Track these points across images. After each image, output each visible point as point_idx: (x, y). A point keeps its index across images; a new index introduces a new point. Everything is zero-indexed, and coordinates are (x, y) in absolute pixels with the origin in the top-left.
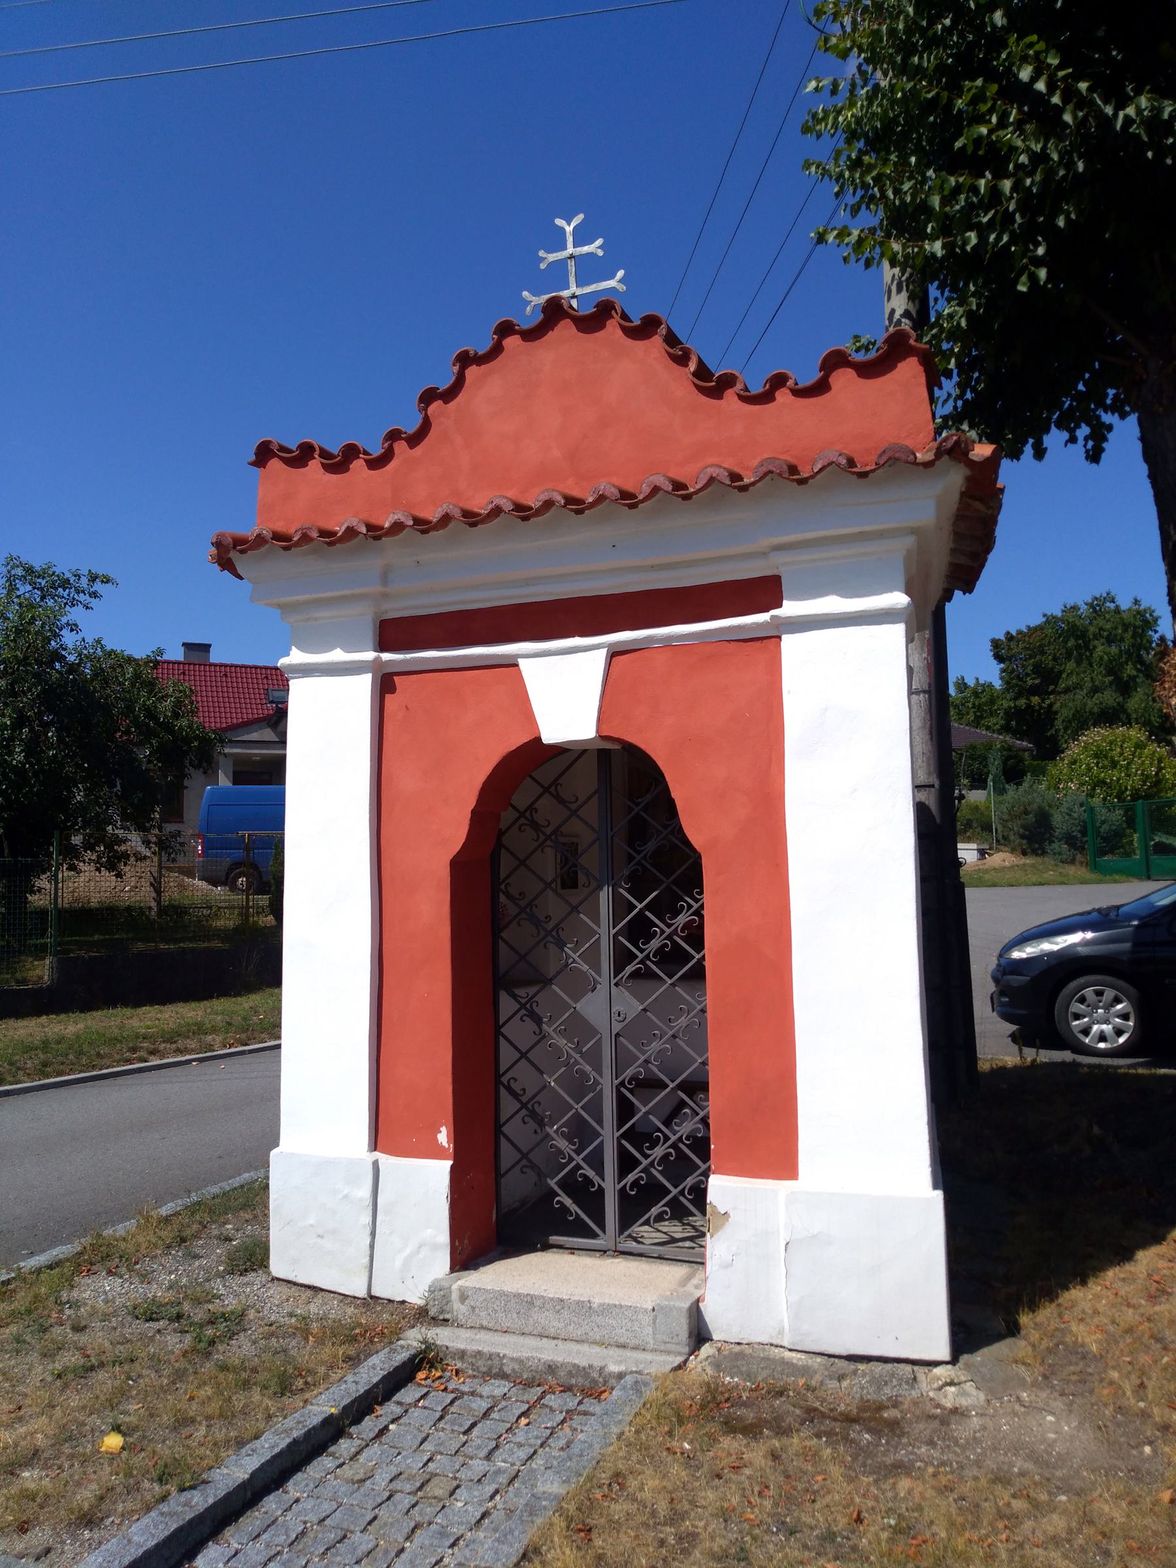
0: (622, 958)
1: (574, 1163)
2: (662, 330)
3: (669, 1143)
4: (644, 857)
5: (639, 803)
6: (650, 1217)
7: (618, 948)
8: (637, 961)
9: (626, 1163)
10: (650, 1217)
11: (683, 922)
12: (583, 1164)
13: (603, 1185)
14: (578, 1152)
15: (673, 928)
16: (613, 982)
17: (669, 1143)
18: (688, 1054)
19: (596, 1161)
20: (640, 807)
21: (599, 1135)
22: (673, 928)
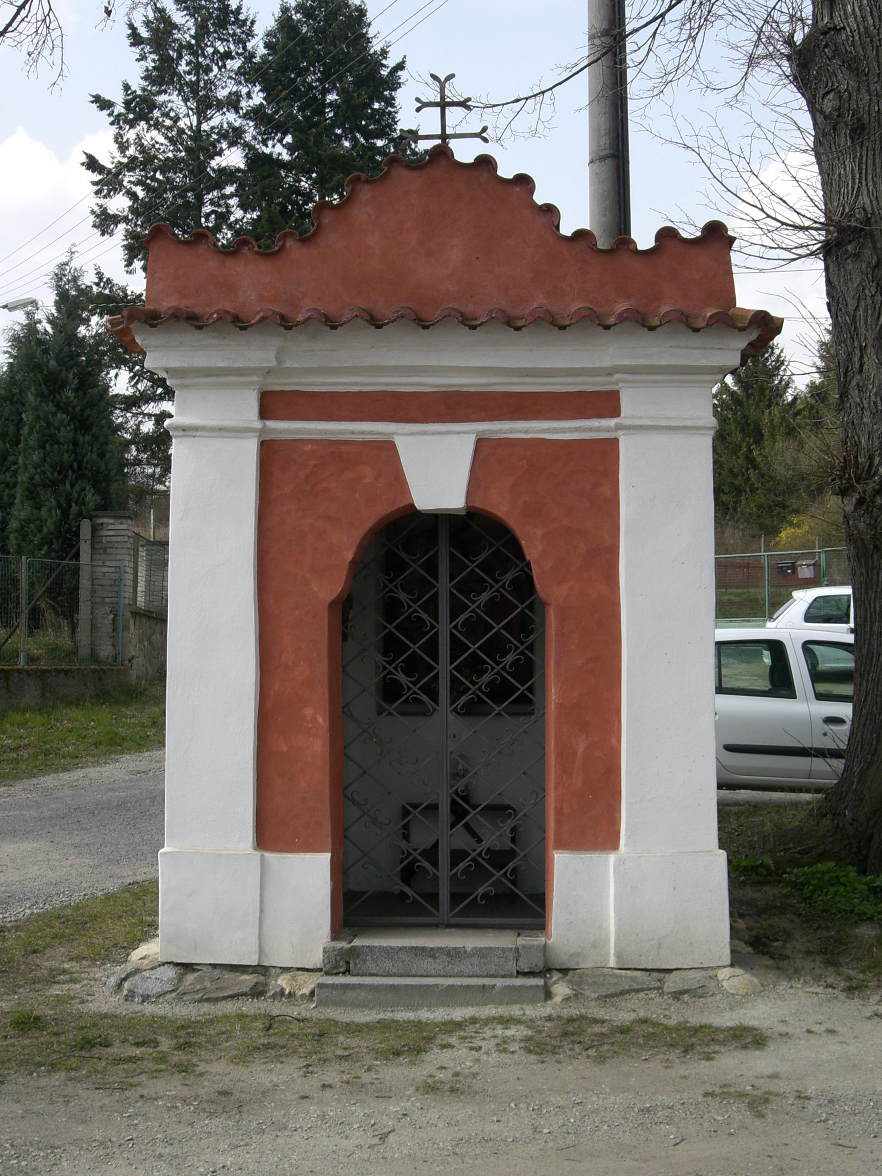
0: (457, 689)
1: (411, 858)
2: (510, 823)
3: (495, 671)
4: (478, 607)
5: (474, 561)
6: (477, 896)
7: (454, 680)
8: (471, 692)
9: (456, 609)
10: (477, 896)
11: (511, 660)
12: (418, 609)
13: (438, 874)
14: (415, 602)
15: (501, 583)
16: (449, 709)
17: (495, 671)
18: (515, 616)
19: (431, 607)
20: (476, 564)
21: (435, 586)
22: (501, 583)
